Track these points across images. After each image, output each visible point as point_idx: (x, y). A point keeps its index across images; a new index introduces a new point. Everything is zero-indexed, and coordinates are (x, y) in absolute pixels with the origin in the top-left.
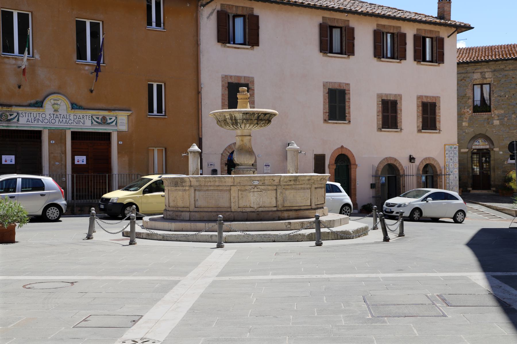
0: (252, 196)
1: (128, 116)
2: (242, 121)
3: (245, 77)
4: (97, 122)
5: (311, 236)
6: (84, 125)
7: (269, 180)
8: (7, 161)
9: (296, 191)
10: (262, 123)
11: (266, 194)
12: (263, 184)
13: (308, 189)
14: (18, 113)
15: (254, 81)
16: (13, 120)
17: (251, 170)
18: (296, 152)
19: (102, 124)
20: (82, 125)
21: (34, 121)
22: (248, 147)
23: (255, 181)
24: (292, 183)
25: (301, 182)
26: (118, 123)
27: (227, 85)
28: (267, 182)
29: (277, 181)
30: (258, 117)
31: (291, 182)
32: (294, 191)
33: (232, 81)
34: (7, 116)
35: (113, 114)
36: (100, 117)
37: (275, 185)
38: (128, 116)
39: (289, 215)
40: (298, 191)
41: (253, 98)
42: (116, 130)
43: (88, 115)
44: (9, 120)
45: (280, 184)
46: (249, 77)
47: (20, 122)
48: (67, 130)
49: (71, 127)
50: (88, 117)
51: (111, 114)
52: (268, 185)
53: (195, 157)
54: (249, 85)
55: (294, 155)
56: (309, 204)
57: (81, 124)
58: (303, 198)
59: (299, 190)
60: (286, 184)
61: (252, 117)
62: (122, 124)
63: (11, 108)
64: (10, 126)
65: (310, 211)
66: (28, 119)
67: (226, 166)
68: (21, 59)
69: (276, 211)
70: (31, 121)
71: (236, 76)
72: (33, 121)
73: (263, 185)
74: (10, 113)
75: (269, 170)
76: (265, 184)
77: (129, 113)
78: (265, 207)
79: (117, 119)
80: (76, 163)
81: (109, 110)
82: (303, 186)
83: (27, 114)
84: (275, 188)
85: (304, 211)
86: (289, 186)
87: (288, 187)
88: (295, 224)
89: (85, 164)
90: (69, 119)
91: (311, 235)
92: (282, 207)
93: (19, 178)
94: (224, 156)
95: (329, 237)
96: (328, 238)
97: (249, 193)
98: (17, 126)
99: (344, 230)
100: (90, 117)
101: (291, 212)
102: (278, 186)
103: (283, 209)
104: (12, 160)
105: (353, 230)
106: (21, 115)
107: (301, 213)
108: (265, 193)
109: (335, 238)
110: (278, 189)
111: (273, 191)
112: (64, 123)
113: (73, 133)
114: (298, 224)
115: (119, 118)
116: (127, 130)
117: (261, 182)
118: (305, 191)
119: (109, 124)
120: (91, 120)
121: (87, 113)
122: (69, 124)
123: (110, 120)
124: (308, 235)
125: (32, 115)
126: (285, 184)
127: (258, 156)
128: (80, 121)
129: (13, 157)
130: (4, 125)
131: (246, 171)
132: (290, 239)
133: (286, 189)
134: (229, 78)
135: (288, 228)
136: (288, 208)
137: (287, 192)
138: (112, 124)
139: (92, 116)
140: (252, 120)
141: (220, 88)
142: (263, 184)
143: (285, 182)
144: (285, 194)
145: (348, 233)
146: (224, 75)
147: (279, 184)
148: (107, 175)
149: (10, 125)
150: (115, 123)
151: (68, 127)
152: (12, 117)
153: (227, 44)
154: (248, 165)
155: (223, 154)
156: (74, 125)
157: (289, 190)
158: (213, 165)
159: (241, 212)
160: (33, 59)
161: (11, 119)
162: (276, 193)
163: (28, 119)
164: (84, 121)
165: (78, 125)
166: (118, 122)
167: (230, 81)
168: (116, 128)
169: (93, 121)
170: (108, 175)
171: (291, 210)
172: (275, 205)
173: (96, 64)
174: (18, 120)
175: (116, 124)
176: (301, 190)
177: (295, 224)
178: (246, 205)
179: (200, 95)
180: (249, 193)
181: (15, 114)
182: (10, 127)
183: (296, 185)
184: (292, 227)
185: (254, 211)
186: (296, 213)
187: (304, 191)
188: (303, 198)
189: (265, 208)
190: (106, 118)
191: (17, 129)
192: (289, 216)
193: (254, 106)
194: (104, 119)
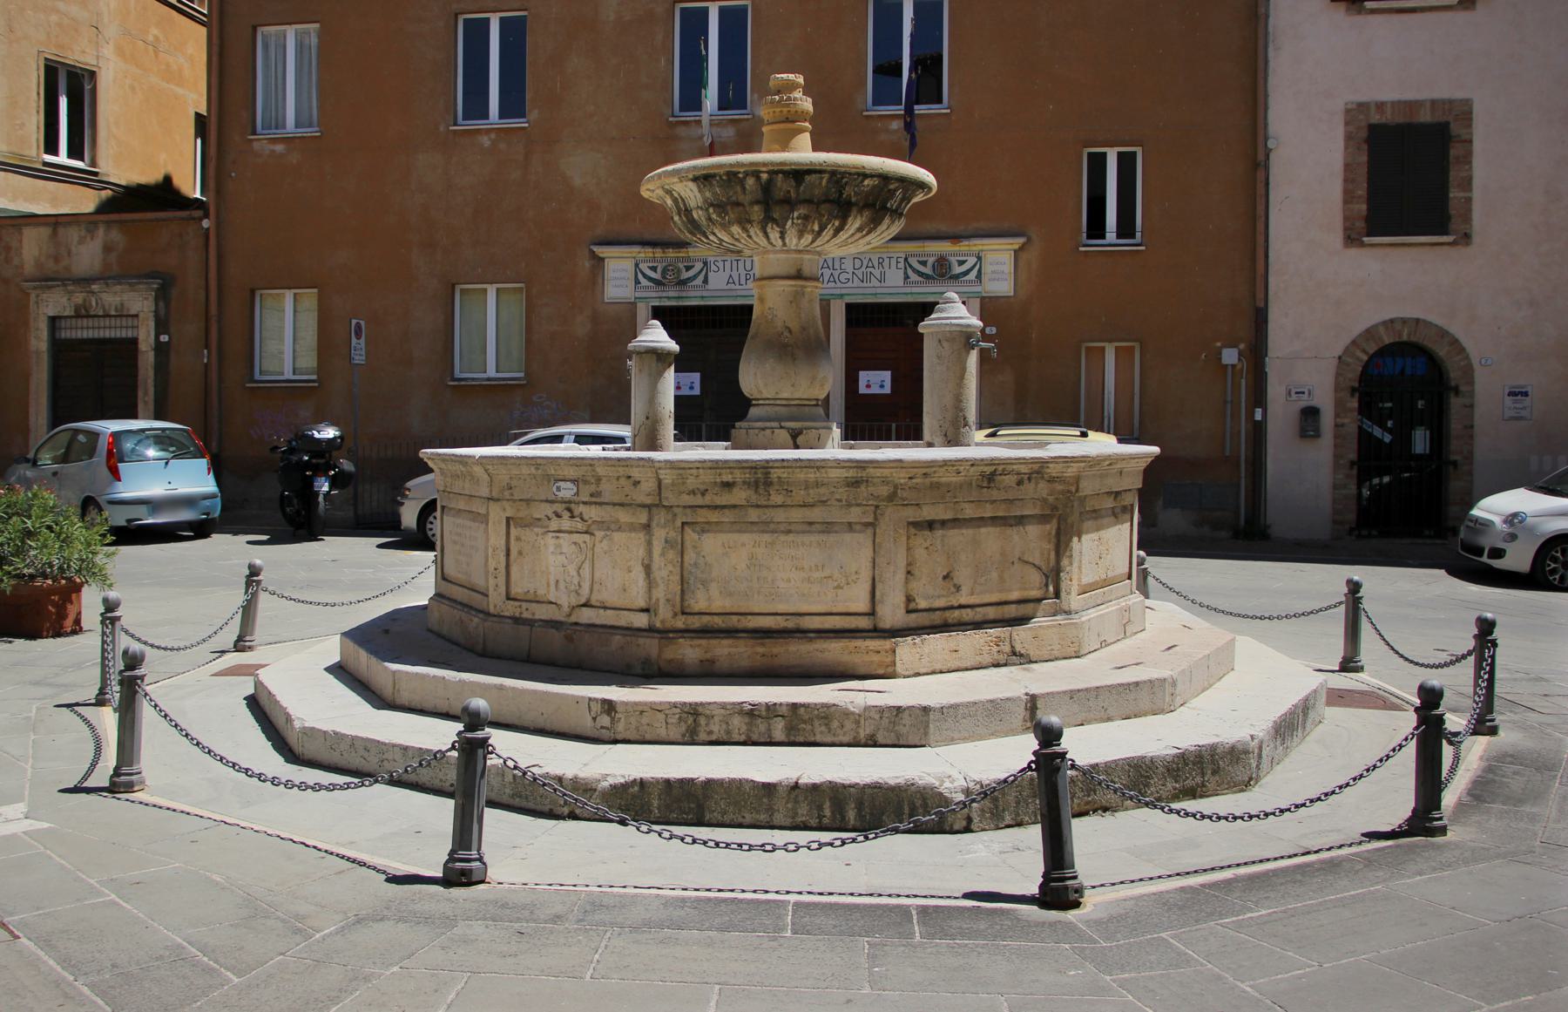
0: (552, 553)
1: (1015, 251)
2: (705, 213)
3: (1433, 102)
4: (920, 274)
5: (634, 796)
6: (883, 284)
7: (618, 478)
8: (683, 387)
9: (767, 537)
10: (796, 214)
11: (606, 548)
12: (594, 499)
13: (858, 527)
14: (705, 263)
15: (1471, 113)
16: (694, 279)
17: (783, 424)
18: (947, 341)
19: (934, 278)
20: (878, 284)
21: (746, 279)
22: (779, 324)
23: (561, 484)
24: (739, 496)
25: (799, 495)
26: (983, 275)
27: (1364, 134)
28: (609, 491)
29: (648, 485)
30: (767, 188)
31: (730, 492)
32: (756, 536)
33: (1384, 120)
34: (679, 271)
35: (967, 248)
36: (931, 260)
37: (644, 506)
38: (1015, 251)
39: (708, 656)
40: (783, 538)
41: (1467, 167)
42: (980, 295)
43: (895, 255)
44: (683, 283)
45: (660, 500)
46: (1451, 102)
47: (710, 286)
48: (832, 301)
49: (844, 291)
50: (893, 262)
51: (962, 248)
52: (614, 505)
53: (640, 370)
54: (1452, 126)
55: (939, 357)
56: (862, 605)
57: (875, 282)
58: (817, 575)
59: (789, 532)
60: (699, 500)
61: (736, 193)
62: (996, 276)
63: (685, 250)
64: (687, 297)
65: (859, 643)
66: (731, 276)
67: (1352, 395)
68: (716, 122)
69: (644, 630)
70: (737, 282)
71: (1399, 102)
72: (743, 282)
73: (596, 503)
74: (686, 264)
75: (1524, 408)
76: (602, 500)
77: (1018, 242)
78: (607, 605)
79: (981, 263)
80: (862, 390)
81: (956, 238)
82: (816, 514)
83: (728, 264)
84: (643, 518)
85: (811, 640)
86: (726, 511)
87: (714, 517)
88: (642, 712)
89: (889, 392)
90: (839, 271)
91: (636, 788)
92: (675, 614)
93: (570, 434)
94: (1348, 365)
95: (770, 810)
96: (763, 817)
97: (542, 534)
98: (702, 297)
99: (892, 782)
100: (899, 260)
101: (725, 642)
102: (654, 510)
103: (680, 623)
104: (884, 384)
105: (971, 785)
106: (713, 268)
107: (834, 650)
108: (605, 542)
109: (820, 817)
110: (654, 524)
111: (633, 534)
112: (825, 282)
113: (850, 308)
114: (661, 716)
115: (989, 258)
116: (1012, 294)
117: (587, 487)
118: (832, 538)
119: (957, 277)
120: (902, 271)
121: (889, 250)
122: (839, 285)
123: (959, 265)
124: (614, 787)
125: (741, 264)
126: (687, 500)
127: (1483, 362)
128: (871, 273)
129: (886, 376)
130: (671, 294)
131: (757, 431)
132: (520, 797)
133: (706, 527)
134: (1373, 109)
135: (602, 727)
136: (718, 622)
137: (711, 544)
138: (966, 278)
139: (906, 259)
140: (738, 204)
141: (1340, 143)
142: (594, 499)
143: (693, 492)
144: (698, 554)
145: (924, 799)
146: (1352, 103)
147: (658, 502)
148: (894, 425)
149: (684, 294)
150: (974, 272)
151: (838, 292)
152: (691, 273)
153: (1366, 3)
154: (778, 402)
155: (1343, 358)
156: (855, 285)
157: (721, 531)
158: (1307, 393)
159: (510, 621)
160: (748, 119)
161: (689, 279)
162: (649, 543)
163: (731, 276)
164: (883, 274)
165: (865, 284)
166: (983, 272)
167: (1376, 118)
168: (978, 289)
169: (910, 271)
170: (897, 426)
171: (730, 633)
172: (642, 604)
173: (902, 112)
174: (706, 281)
175: (979, 276)
176: (809, 532)
177: (642, 712)
178: (532, 592)
179: (1260, 175)
180: (542, 534)
181: (699, 266)
182: (685, 299)
183: (766, 506)
184: (621, 727)
185: (563, 619)
186: (761, 650)
187: (823, 537)
188: (817, 575)
189: (602, 611)
190: (947, 260)
191: (702, 303)
192: (713, 662)
193: (1467, 195)
194: (942, 265)
